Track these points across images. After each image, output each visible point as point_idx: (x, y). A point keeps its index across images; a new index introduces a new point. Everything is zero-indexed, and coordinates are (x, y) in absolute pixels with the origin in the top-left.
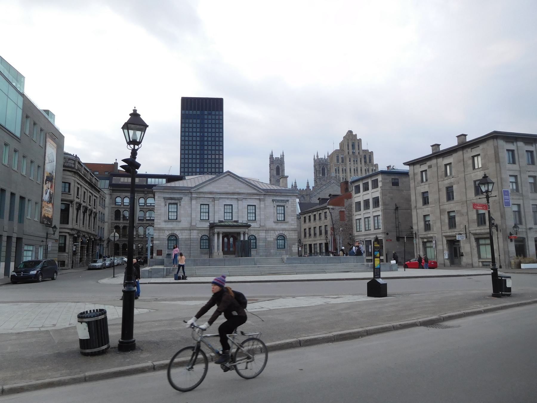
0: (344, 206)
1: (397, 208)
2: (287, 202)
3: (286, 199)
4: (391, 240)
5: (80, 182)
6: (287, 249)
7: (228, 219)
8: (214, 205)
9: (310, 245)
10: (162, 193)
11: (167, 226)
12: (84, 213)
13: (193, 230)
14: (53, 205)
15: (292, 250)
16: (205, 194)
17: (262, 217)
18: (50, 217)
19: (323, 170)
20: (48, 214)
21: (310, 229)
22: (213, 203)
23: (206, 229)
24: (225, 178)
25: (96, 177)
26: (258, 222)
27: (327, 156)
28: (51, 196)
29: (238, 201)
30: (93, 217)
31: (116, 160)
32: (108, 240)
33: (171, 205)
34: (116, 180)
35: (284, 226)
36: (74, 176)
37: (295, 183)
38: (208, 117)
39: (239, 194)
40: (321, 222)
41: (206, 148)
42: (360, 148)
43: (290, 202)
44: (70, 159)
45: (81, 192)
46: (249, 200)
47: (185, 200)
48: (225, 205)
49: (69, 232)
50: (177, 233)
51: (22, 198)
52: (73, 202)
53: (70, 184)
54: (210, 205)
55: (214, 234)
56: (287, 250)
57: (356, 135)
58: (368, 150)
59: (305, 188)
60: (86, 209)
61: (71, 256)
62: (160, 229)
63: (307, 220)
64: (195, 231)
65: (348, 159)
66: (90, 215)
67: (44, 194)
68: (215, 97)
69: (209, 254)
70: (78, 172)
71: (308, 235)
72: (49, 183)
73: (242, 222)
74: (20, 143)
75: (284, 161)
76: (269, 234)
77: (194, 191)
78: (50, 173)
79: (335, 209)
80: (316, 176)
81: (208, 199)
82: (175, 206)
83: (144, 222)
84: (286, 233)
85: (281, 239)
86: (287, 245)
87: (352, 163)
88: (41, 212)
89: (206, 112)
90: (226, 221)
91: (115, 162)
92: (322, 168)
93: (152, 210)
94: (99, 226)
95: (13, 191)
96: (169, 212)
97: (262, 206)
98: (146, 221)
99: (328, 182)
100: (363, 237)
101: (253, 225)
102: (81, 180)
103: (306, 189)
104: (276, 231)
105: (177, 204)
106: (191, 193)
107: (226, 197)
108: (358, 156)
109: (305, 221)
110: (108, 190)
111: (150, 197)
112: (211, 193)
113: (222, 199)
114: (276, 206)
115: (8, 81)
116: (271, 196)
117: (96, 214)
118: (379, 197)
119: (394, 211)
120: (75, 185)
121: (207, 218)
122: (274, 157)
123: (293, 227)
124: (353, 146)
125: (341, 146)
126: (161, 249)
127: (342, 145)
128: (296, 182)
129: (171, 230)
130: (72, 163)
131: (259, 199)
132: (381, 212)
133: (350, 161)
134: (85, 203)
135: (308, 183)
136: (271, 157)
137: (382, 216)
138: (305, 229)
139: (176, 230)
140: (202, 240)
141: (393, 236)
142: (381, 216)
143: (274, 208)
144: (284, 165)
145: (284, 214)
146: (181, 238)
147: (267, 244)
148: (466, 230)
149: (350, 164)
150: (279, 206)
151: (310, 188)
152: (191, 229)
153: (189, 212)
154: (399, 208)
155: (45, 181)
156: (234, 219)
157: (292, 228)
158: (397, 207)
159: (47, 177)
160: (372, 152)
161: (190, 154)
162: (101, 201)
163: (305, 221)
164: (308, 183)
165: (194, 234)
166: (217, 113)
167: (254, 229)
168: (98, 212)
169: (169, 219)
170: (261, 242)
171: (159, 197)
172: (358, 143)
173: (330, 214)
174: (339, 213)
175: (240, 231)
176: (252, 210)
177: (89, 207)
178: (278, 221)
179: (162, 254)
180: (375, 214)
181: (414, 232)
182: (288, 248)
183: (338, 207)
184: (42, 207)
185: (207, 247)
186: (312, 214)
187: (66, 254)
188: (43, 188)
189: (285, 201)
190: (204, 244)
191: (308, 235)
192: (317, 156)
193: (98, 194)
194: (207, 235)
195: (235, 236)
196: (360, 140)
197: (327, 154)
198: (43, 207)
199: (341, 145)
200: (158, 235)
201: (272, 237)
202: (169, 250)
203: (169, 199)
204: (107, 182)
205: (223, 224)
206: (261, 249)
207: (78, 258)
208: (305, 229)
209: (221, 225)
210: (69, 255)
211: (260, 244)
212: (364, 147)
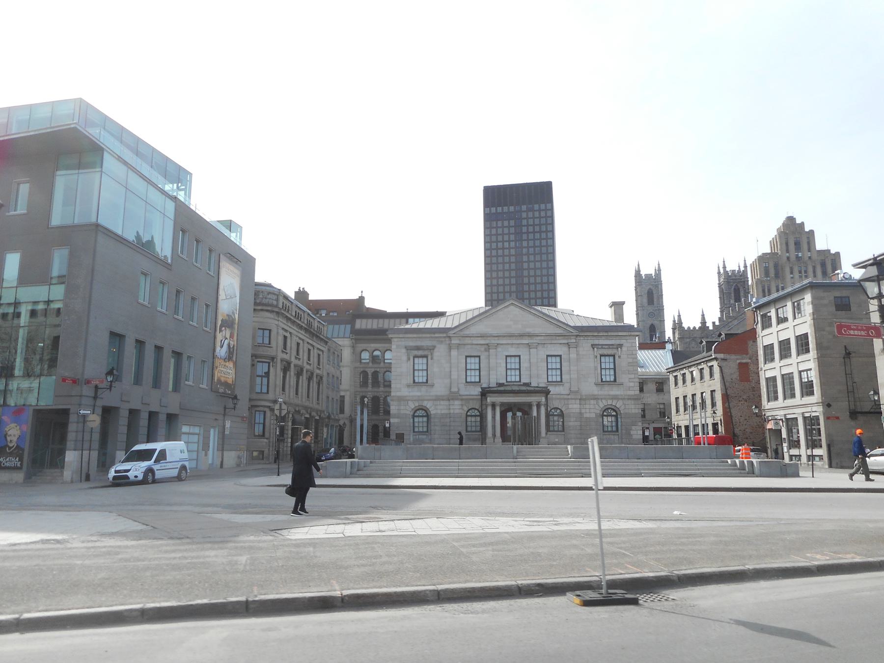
0: (747, 354)
1: (848, 354)
2: (619, 349)
3: (618, 342)
4: (837, 418)
5: (288, 327)
7: (513, 380)
8: (489, 357)
9: (687, 427)
10: (403, 340)
11: (412, 394)
13: (453, 399)
14: (235, 364)
16: (473, 339)
17: (574, 376)
18: (230, 381)
19: (737, 291)
20: (227, 378)
21: (685, 397)
22: (487, 353)
23: (475, 397)
24: (506, 310)
25: (319, 320)
26: (567, 385)
27: (743, 266)
28: (231, 350)
29: (530, 348)
30: (315, 383)
31: (362, 292)
32: (350, 418)
33: (470, 358)
34: (360, 324)
35: (615, 391)
36: (277, 318)
37: (679, 316)
39: (530, 336)
40: (703, 385)
41: (525, 266)
42: (812, 248)
43: (624, 349)
44: (269, 293)
45: (292, 344)
46: (549, 346)
47: (440, 351)
49: (270, 406)
50: (428, 405)
51: (178, 355)
52: (275, 359)
53: (270, 330)
56: (622, 435)
57: (803, 223)
58: (829, 251)
59: (698, 325)
61: (273, 444)
62: (401, 399)
63: (680, 382)
64: (457, 402)
65: (788, 270)
67: (218, 349)
69: (481, 442)
71: (682, 409)
72: (228, 330)
73: (537, 385)
74: (171, 270)
76: (587, 406)
77: (454, 334)
78: (228, 315)
79: (728, 361)
80: (723, 304)
81: (479, 346)
82: (425, 360)
84: (619, 404)
85: (421, 416)
86: (621, 425)
88: (213, 376)
89: (524, 208)
90: (509, 384)
91: (360, 296)
92: (735, 289)
94: (328, 397)
95: (159, 344)
98: (384, 387)
100: (782, 412)
102: (289, 324)
103: (700, 328)
104: (600, 401)
106: (450, 337)
107: (509, 342)
110: (348, 339)
112: (482, 336)
113: (502, 346)
115: (146, 179)
117: (321, 378)
118: (807, 333)
119: (843, 360)
120: (278, 333)
121: (477, 380)
122: (643, 273)
123: (632, 393)
124: (797, 244)
125: (773, 246)
127: (774, 245)
128: (681, 314)
129: (418, 400)
130: (273, 299)
131: (568, 343)
132: (814, 362)
133: (792, 273)
134: (299, 360)
135: (703, 315)
136: (638, 274)
137: (815, 370)
138: (677, 399)
140: (470, 418)
141: (842, 407)
143: (596, 359)
145: (615, 369)
146: (434, 414)
147: (583, 424)
148: (786, 393)
150: (605, 356)
151: (707, 325)
152: (452, 396)
153: (448, 370)
154: (853, 355)
155: (218, 327)
156: (523, 381)
157: (629, 395)
158: (847, 351)
159: (222, 320)
162: (331, 357)
164: (703, 315)
165: (456, 407)
166: (543, 206)
168: (325, 374)
169: (414, 382)
171: (398, 346)
172: (808, 238)
173: (718, 368)
174: (737, 367)
175: (531, 401)
176: (554, 363)
177: (307, 367)
178: (602, 383)
182: (623, 431)
183: (736, 357)
184: (213, 368)
185: (478, 429)
187: (265, 440)
188: (215, 337)
189: (615, 347)
190: (421, 425)
192: (724, 267)
193: (325, 346)
194: (477, 408)
195: (526, 410)
196: (812, 232)
197: (744, 262)
198: (217, 367)
200: (398, 410)
201: (592, 410)
202: (415, 434)
204: (349, 327)
205: (502, 388)
207: (287, 446)
208: (677, 399)
209: (501, 389)
210: (269, 442)
212: (820, 245)
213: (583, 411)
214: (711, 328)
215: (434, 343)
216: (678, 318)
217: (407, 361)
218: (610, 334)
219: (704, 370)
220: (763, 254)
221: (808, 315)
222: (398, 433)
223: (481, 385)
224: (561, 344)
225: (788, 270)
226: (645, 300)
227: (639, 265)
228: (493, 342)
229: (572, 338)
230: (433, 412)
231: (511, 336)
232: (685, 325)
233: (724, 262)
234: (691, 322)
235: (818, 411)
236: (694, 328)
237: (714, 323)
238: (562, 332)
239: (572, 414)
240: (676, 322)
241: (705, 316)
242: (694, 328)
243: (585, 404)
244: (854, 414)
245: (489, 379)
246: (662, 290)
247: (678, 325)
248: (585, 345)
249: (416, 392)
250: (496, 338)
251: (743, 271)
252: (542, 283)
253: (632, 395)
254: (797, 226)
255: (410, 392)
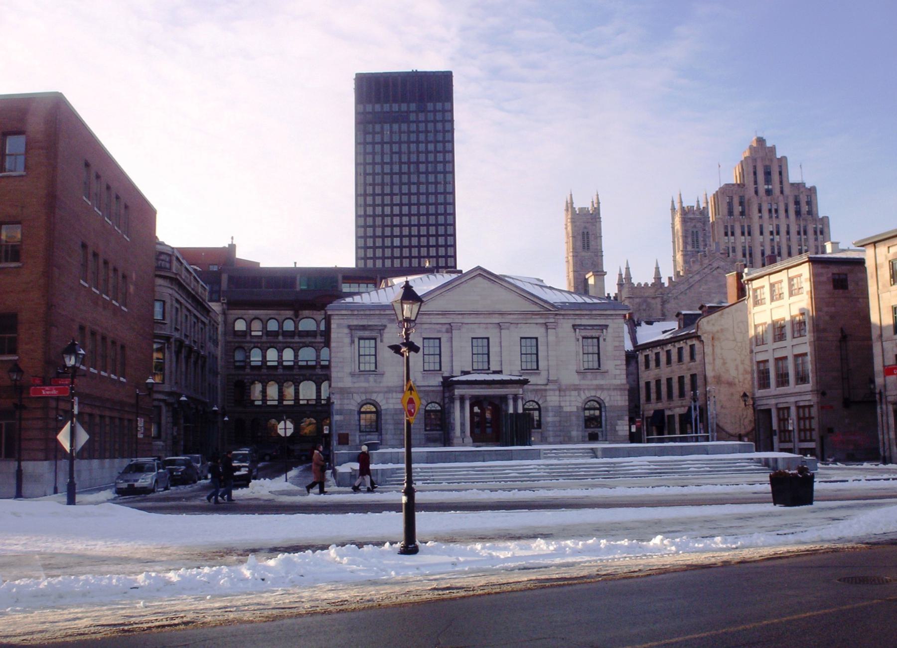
4: (831, 407)
6: (606, 428)
8: (451, 340)
10: (346, 318)
11: (356, 385)
12: (188, 358)
15: (616, 431)
22: (449, 335)
24: (472, 282)
29: (501, 329)
31: (232, 238)
37: (628, 269)
38: (417, 116)
42: (784, 179)
43: (609, 330)
46: (523, 326)
48: (473, 338)
49: (165, 400)
50: (379, 398)
54: (442, 340)
55: (452, 400)
59: (651, 281)
60: (190, 349)
62: (343, 391)
63: (652, 364)
65: (755, 209)
66: (196, 363)
68: (443, 70)
70: (178, 277)
71: (653, 396)
75: (601, 216)
76: (567, 398)
83: (295, 372)
84: (604, 396)
86: (606, 420)
87: (766, 214)
91: (230, 243)
93: (310, 345)
96: (359, 355)
97: (552, 338)
99: (705, 266)
101: (533, 379)
105: (375, 339)
108: (781, 198)
109: (647, 366)
111: (305, 316)
112: (444, 314)
114: (581, 339)
116: (570, 317)
122: (577, 205)
124: (768, 174)
126: (346, 432)
128: (630, 266)
129: (366, 393)
132: (810, 345)
133: (760, 211)
135: (657, 268)
136: (570, 206)
139: (376, 392)
142: (809, 354)
144: (600, 224)
145: (599, 354)
149: (761, 217)
151: (662, 281)
156: (493, 368)
160: (813, 190)
161: (397, 236)
163: (647, 366)
164: (657, 268)
166: (439, 106)
167: (535, 387)
170: (551, 414)
171: (339, 326)
177: (187, 342)
179: (349, 442)
180: (798, 351)
181: (877, 391)
186: (663, 349)
191: (653, 396)
194: (437, 401)
199: (716, 197)
201: (572, 403)
203: (360, 330)
206: (550, 429)
211: (549, 418)
212: (794, 177)
213: (562, 404)
214: (666, 285)
215: (384, 321)
216: (626, 271)
217: (351, 345)
218: (594, 312)
219: (684, 350)
220: (726, 185)
221: (805, 293)
222: (341, 434)
223: (442, 374)
224: (537, 324)
225: (755, 209)
226: (579, 243)
227: (571, 195)
228: (457, 321)
229: (551, 316)
230: (384, 406)
231: (477, 314)
232: (635, 281)
233: (680, 195)
234: (643, 277)
235: (810, 399)
236: (646, 284)
237: (670, 278)
238: (539, 309)
239: (550, 408)
240: (624, 276)
241: (660, 269)
242: (646, 284)
243: (565, 396)
244: (847, 403)
245: (452, 366)
246: (600, 229)
247: (624, 282)
248: (566, 325)
249: (362, 384)
250: (460, 317)
251: (704, 208)
252: (437, 215)
253: (618, 385)
254: (767, 151)
255: (354, 382)
